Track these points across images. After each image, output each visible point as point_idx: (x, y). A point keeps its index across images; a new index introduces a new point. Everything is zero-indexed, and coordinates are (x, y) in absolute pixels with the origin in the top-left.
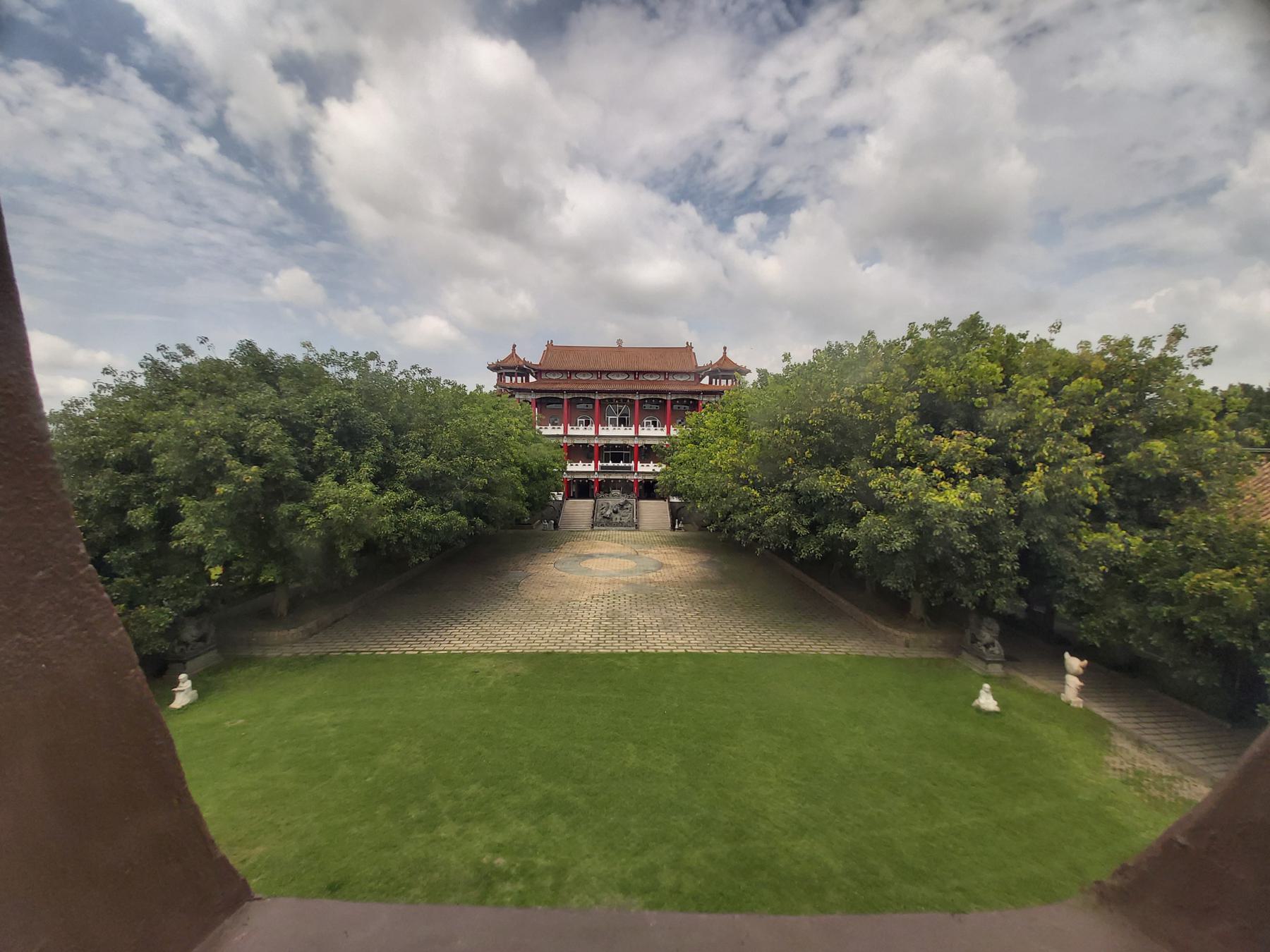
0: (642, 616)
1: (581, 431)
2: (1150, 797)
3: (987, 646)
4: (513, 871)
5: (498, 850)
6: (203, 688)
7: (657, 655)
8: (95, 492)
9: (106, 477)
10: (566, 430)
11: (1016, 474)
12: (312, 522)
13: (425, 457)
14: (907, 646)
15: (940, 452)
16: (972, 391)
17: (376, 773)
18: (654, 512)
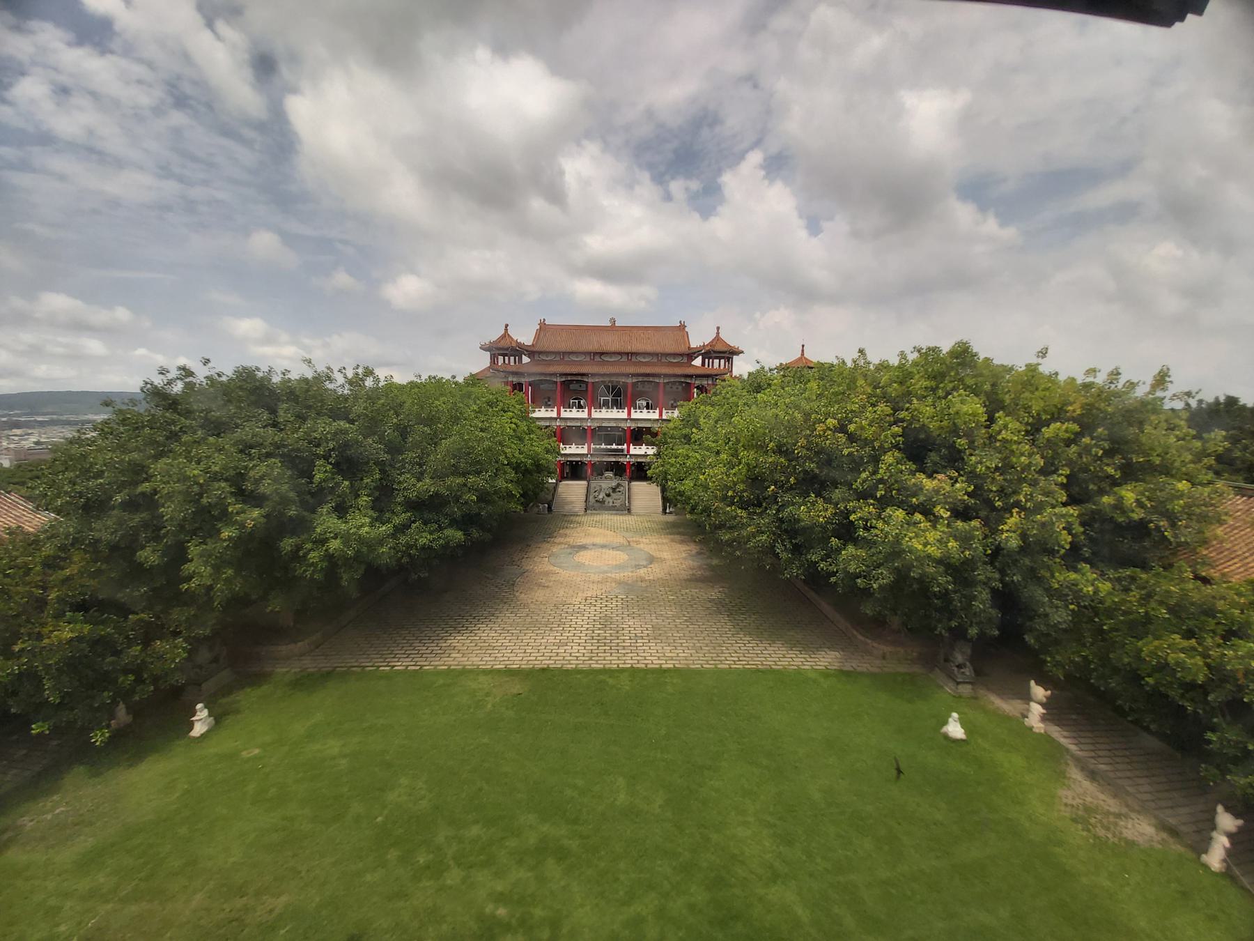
0: (632, 625)
1: (574, 413)
2: (1096, 837)
3: (959, 667)
4: (514, 921)
5: (500, 898)
6: (219, 718)
7: (647, 671)
8: (106, 536)
9: (114, 519)
10: (559, 413)
11: (992, 522)
12: (314, 556)
13: (419, 480)
14: (884, 658)
15: (921, 489)
16: (955, 431)
17: (386, 812)
18: (646, 495)
